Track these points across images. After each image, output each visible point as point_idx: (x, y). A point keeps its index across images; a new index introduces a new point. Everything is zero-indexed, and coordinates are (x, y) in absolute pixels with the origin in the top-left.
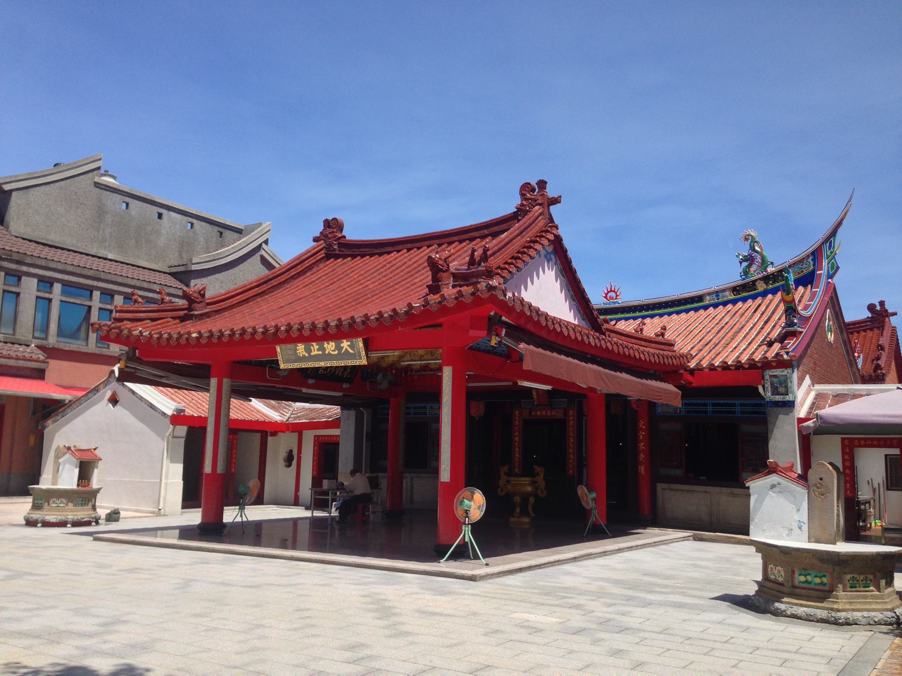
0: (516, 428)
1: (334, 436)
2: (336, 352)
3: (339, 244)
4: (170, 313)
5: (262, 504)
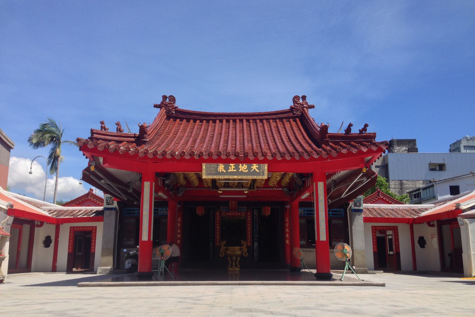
0: (217, 222)
1: (87, 227)
2: (247, 171)
3: (176, 111)
4: (125, 139)
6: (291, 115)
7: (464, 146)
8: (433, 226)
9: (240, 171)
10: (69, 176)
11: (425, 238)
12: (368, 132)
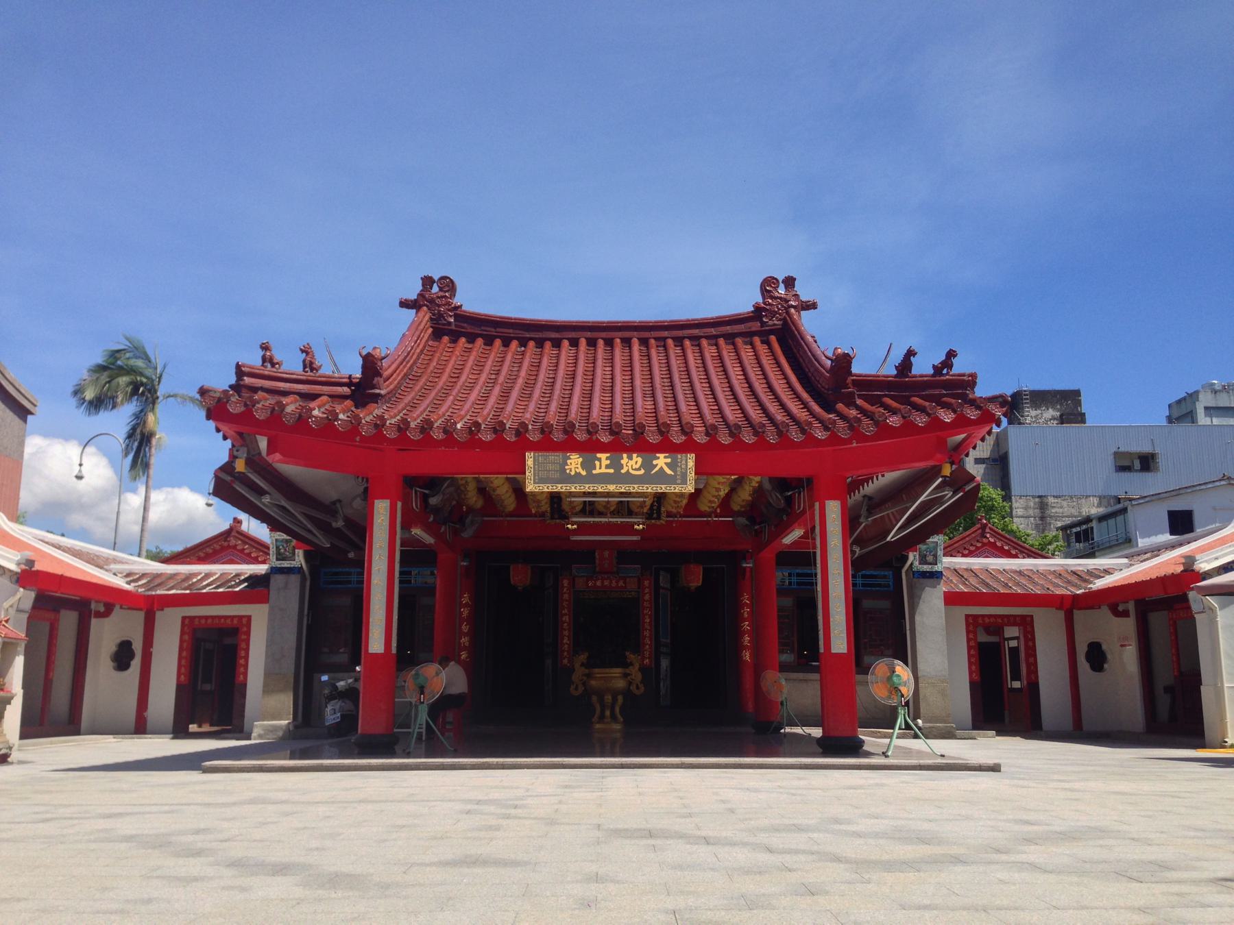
2: (642, 472)
3: (456, 316)
5: (77, 732)
6: (755, 326)
7: (1206, 408)
8: (1125, 614)
10: (179, 484)
11: (1104, 647)
12: (955, 370)
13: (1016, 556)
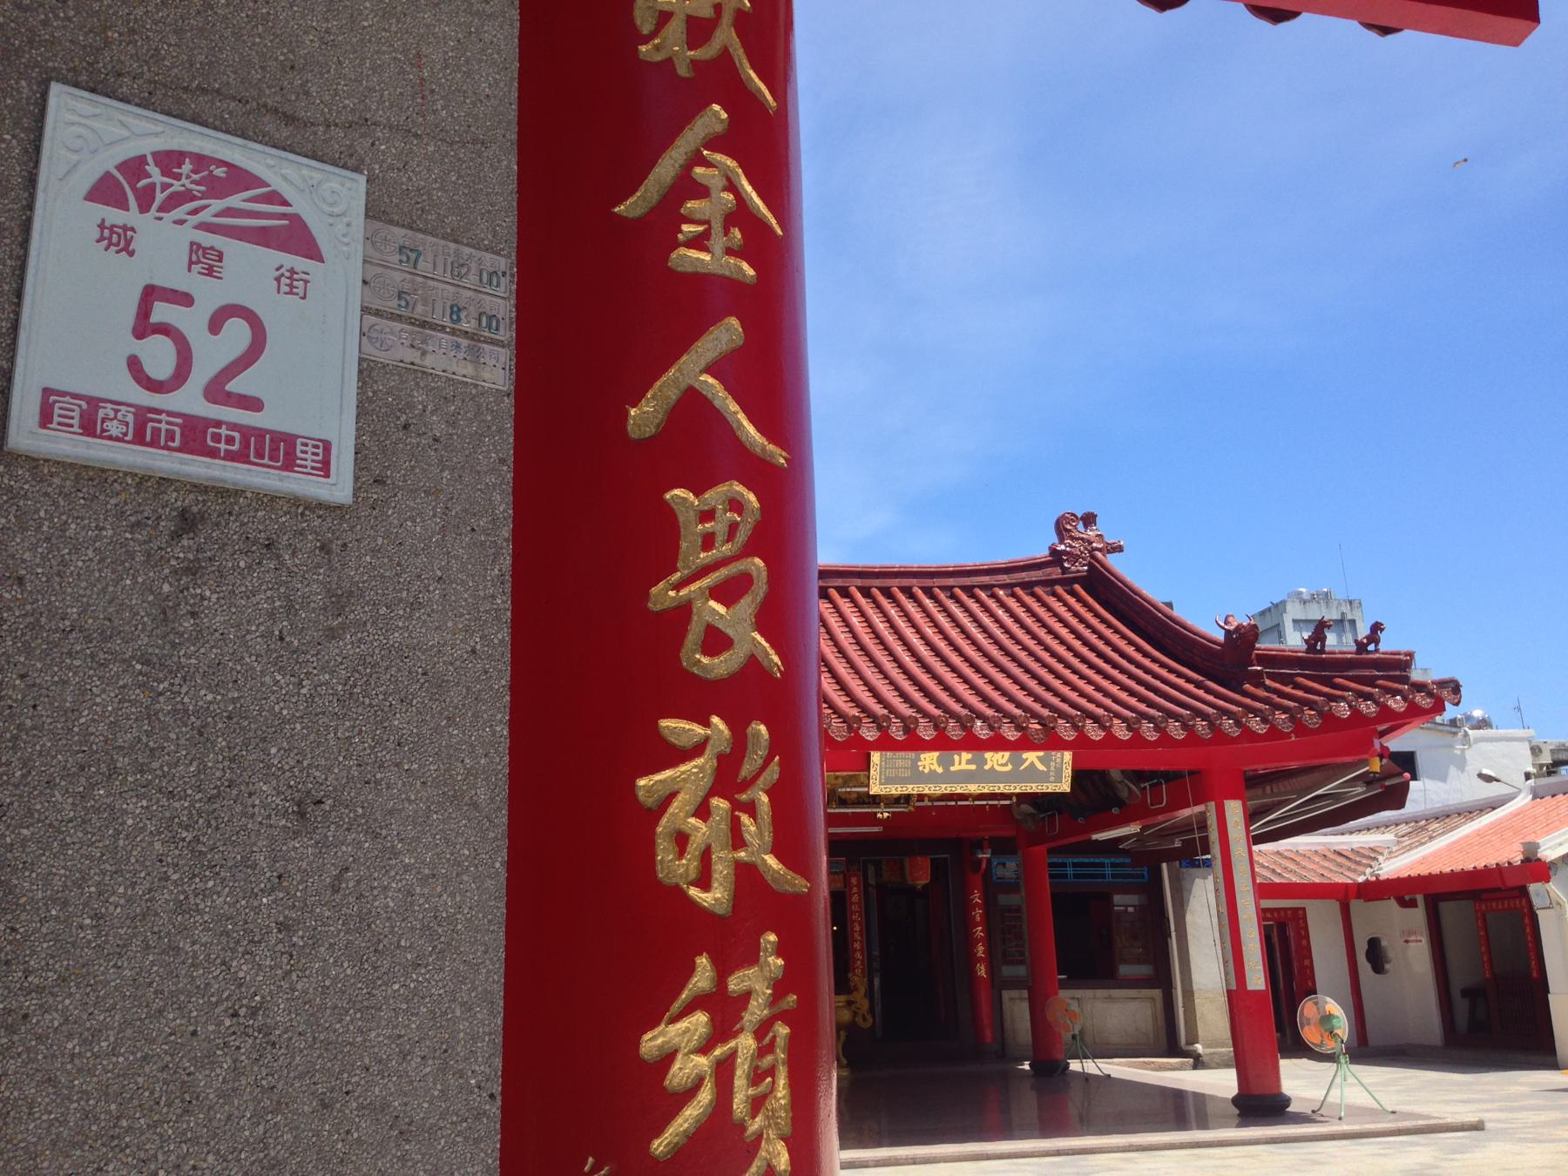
2: (1009, 767)
6: (1056, 573)
7: (1295, 621)
8: (1412, 904)
9: (986, 767)
10: (654, 833)
11: (1384, 943)
12: (1383, 647)
13: (1023, 797)
